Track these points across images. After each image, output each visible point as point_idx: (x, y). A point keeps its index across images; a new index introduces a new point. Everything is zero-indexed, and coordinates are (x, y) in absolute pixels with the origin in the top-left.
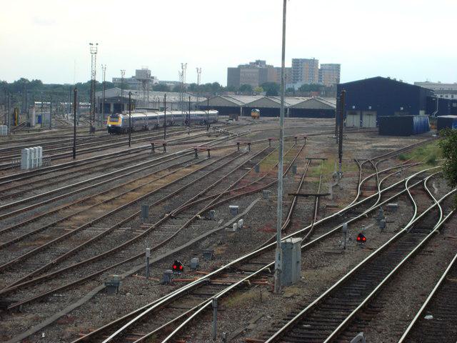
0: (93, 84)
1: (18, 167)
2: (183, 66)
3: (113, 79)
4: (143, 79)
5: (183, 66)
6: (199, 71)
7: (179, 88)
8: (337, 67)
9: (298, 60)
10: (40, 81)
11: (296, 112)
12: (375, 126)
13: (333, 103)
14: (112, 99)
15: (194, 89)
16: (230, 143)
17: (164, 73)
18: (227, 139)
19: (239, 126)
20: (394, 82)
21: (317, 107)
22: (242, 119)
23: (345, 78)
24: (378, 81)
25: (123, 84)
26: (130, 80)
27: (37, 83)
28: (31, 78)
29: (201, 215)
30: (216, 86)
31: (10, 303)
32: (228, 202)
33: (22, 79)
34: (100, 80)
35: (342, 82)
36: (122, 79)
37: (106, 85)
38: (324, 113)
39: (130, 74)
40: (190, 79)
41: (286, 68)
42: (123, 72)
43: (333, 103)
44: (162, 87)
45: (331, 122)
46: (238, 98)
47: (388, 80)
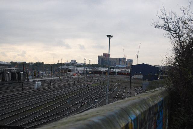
0: (59, 63)
1: (33, 88)
2: (85, 59)
3: (104, 54)
4: (74, 63)
5: (85, 59)
6: (90, 61)
7: (84, 65)
8: (99, 56)
9: (100, 56)
10: (43, 63)
11: (119, 73)
12: (142, 78)
13: (129, 71)
14: (64, 69)
15: (89, 66)
16: (98, 82)
17: (80, 61)
18: (97, 81)
19: (102, 77)
20: (148, 65)
21: (124, 72)
22: (102, 75)
23: (134, 63)
24: (144, 64)
25: (67, 64)
26: (70, 63)
27: (42, 63)
28: (40, 62)
29: (86, 103)
30: (96, 64)
31: (25, 127)
32: (95, 99)
33: (38, 62)
34: (60, 62)
35: (133, 64)
36: (67, 63)
37: (63, 64)
38: (127, 74)
39: (69, 62)
40: (87, 63)
41: (110, 58)
42: (67, 61)
43: (129, 71)
44: (80, 65)
45: (129, 77)
46: (102, 69)
47: (146, 64)
